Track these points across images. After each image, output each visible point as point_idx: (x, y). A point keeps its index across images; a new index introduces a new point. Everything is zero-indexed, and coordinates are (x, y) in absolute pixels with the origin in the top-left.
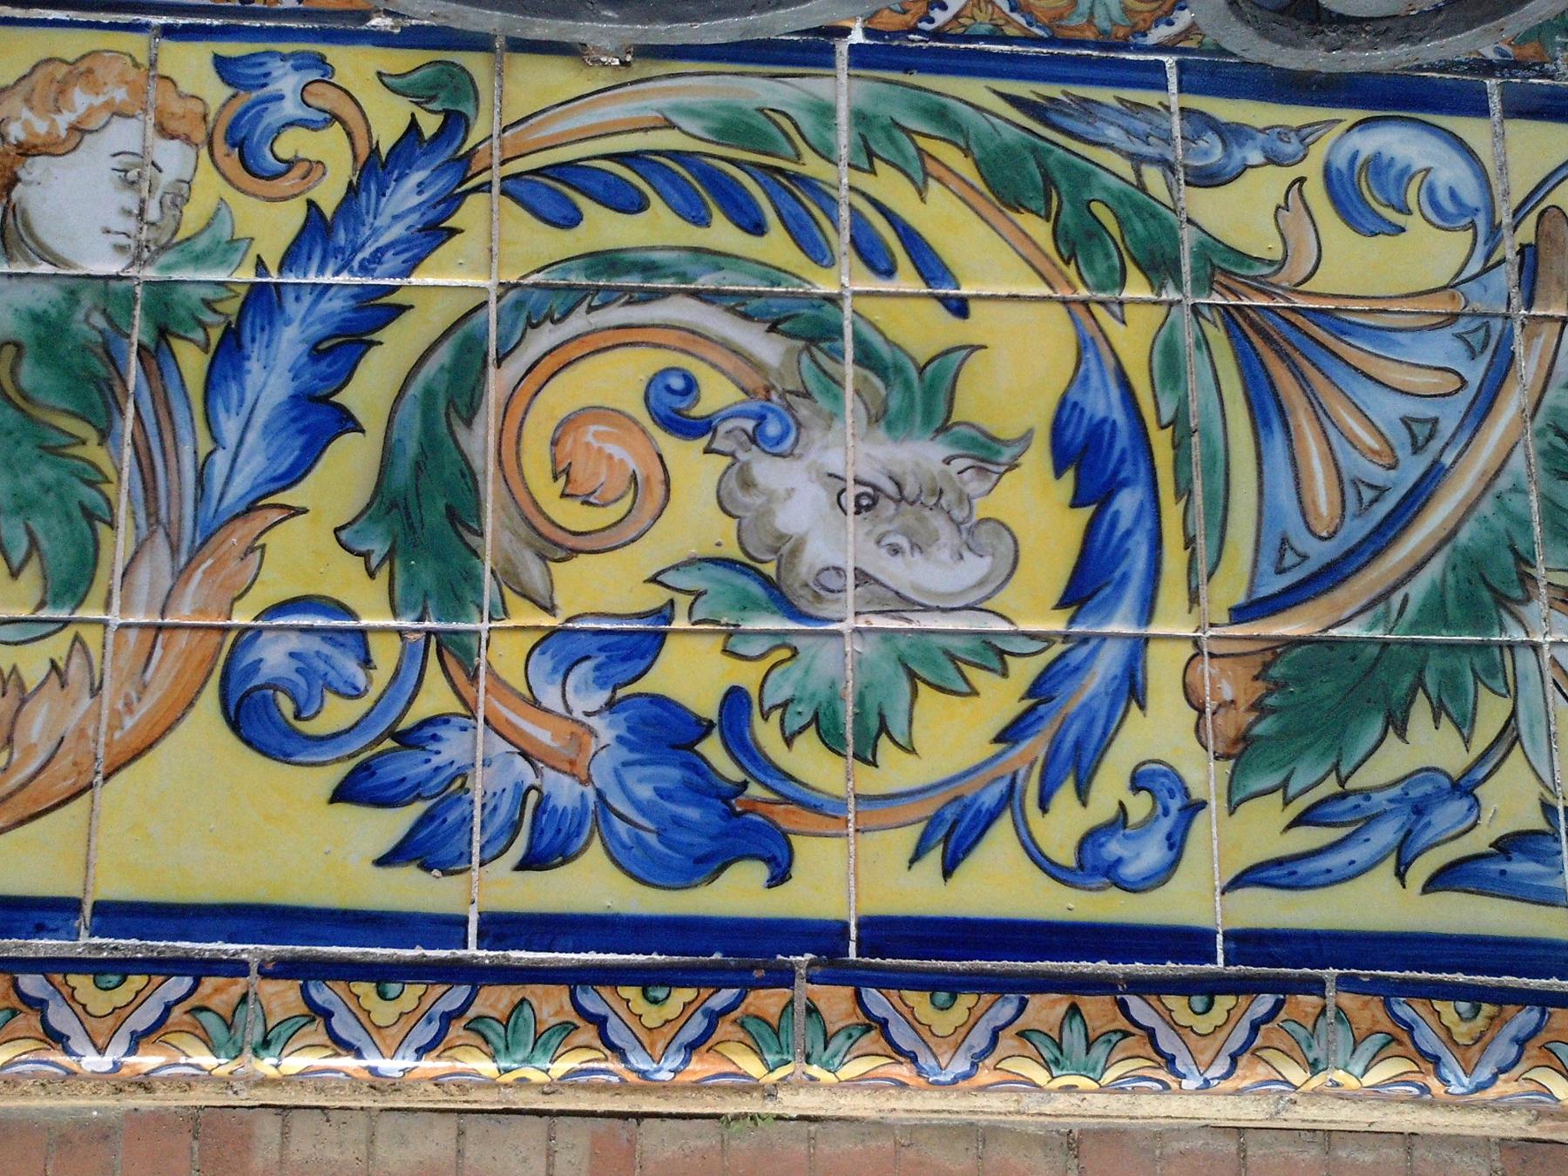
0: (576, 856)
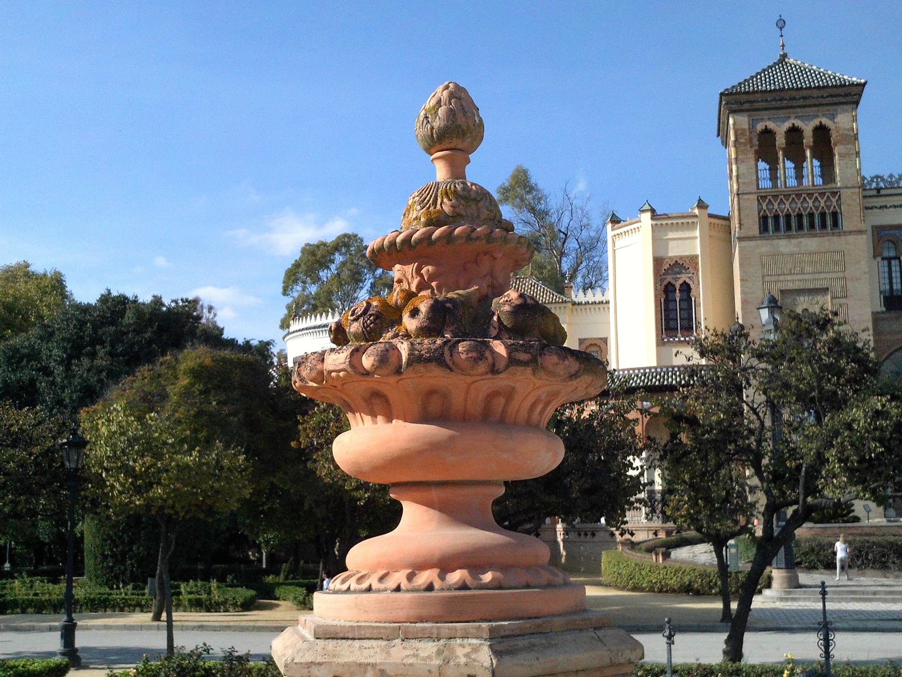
0: (506, 483)
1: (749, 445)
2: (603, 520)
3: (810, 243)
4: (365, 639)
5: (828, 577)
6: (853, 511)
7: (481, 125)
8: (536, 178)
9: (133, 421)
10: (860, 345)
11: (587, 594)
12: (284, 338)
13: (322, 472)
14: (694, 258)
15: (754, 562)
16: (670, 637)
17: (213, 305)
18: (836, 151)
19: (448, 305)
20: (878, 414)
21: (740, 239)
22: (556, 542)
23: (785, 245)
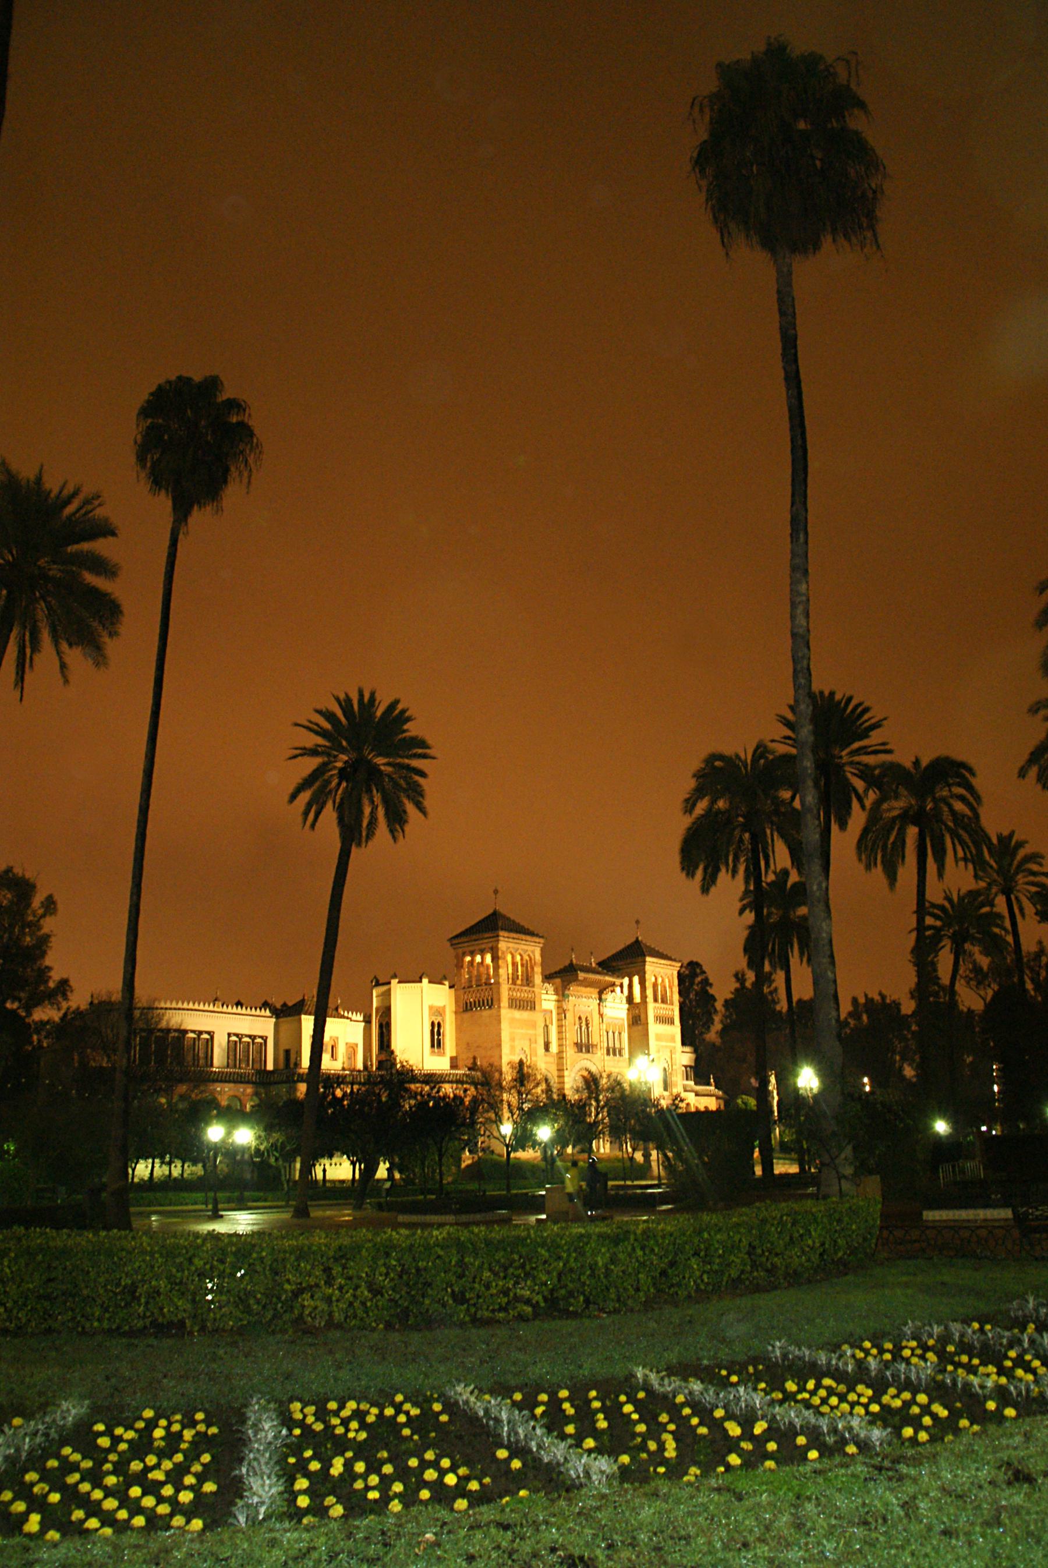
1: (943, 1381)
2: (431, 1104)
4: (793, 380)
5: (38, 895)
6: (1020, 845)
7: (745, 950)
8: (56, 898)
9: (981, 1329)
10: (314, 1248)
11: (776, 1172)
12: (297, 725)
13: (791, 1082)
14: (511, 1006)
15: (27, 1520)
16: (600, 993)
17: (243, 500)
19: (717, 763)
20: (751, 1531)
21: (508, 1189)
22: (898, 834)
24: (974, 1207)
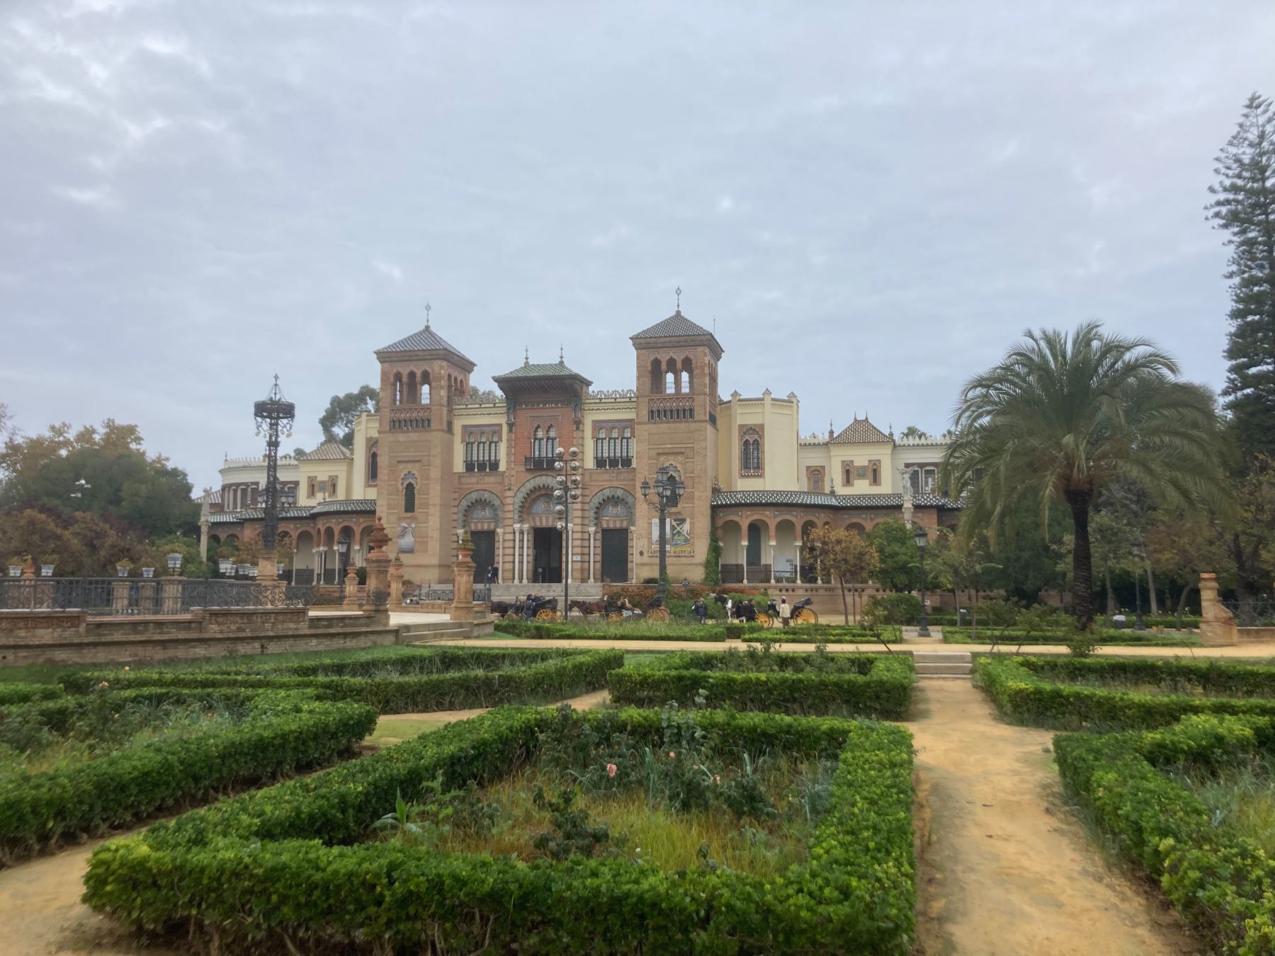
3: (413, 436)
18: (589, 419)
23: (401, 437)
24: (452, 707)
